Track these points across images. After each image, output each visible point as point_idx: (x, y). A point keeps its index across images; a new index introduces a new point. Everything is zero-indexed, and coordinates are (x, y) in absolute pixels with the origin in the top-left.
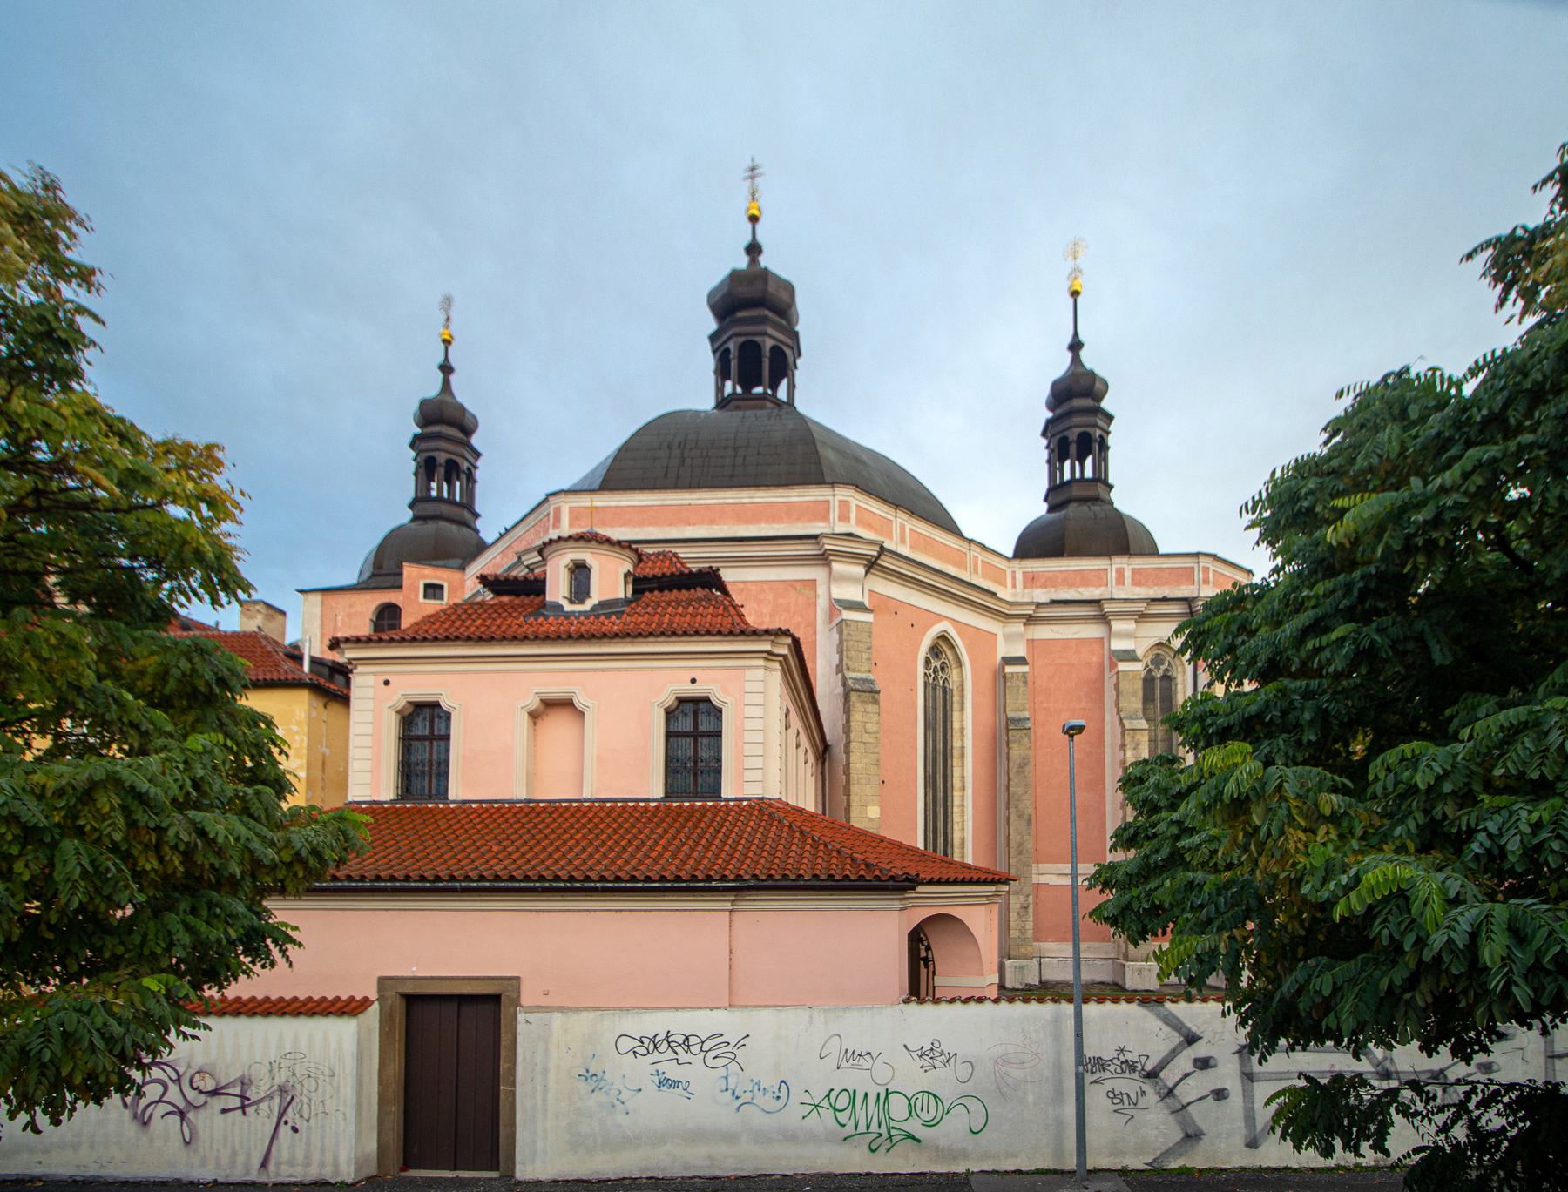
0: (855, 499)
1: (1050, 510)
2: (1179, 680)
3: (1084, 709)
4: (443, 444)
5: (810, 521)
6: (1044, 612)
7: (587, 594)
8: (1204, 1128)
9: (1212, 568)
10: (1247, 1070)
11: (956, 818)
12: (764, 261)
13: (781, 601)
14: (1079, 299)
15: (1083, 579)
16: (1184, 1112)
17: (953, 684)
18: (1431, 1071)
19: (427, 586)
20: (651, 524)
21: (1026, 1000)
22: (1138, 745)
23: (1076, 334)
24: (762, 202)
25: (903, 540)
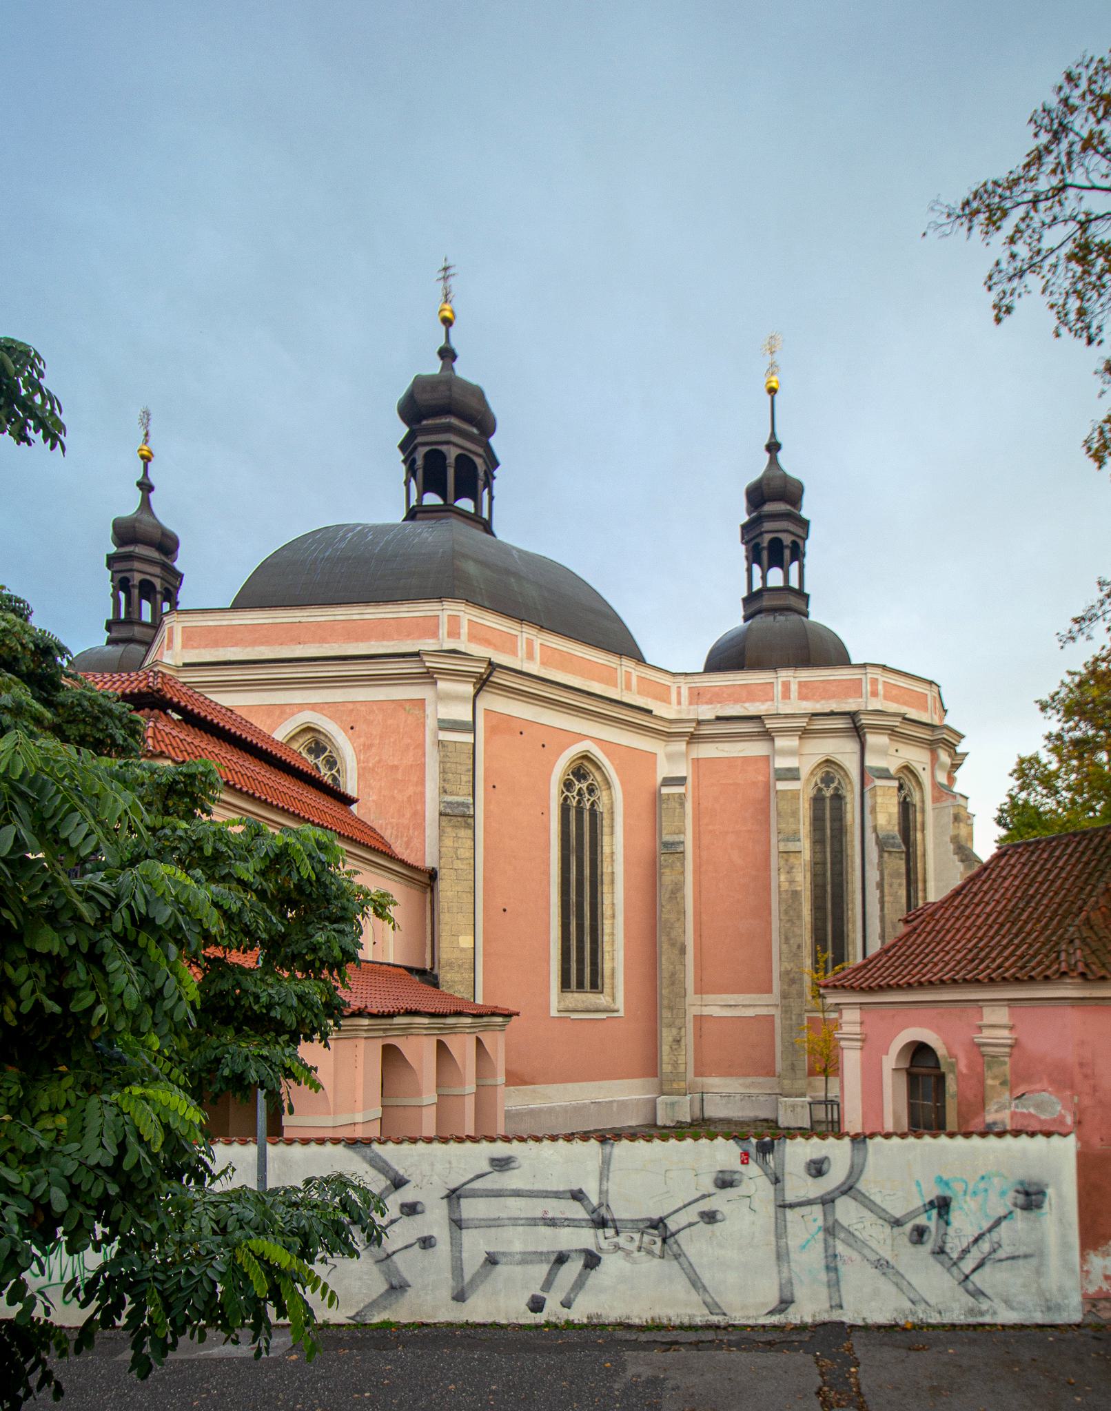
0: (466, 614)
1: (746, 619)
2: (848, 799)
3: (749, 831)
4: (137, 565)
5: (420, 637)
8: (408, 1277)
9: (881, 679)
10: (456, 1217)
11: (607, 948)
12: (462, 370)
13: (390, 722)
14: (777, 397)
15: (750, 694)
16: (389, 1261)
17: (601, 808)
18: (650, 1220)
20: (262, 644)
21: (680, 1138)
22: (792, 868)
23: (773, 434)
24: (457, 304)
25: (530, 656)
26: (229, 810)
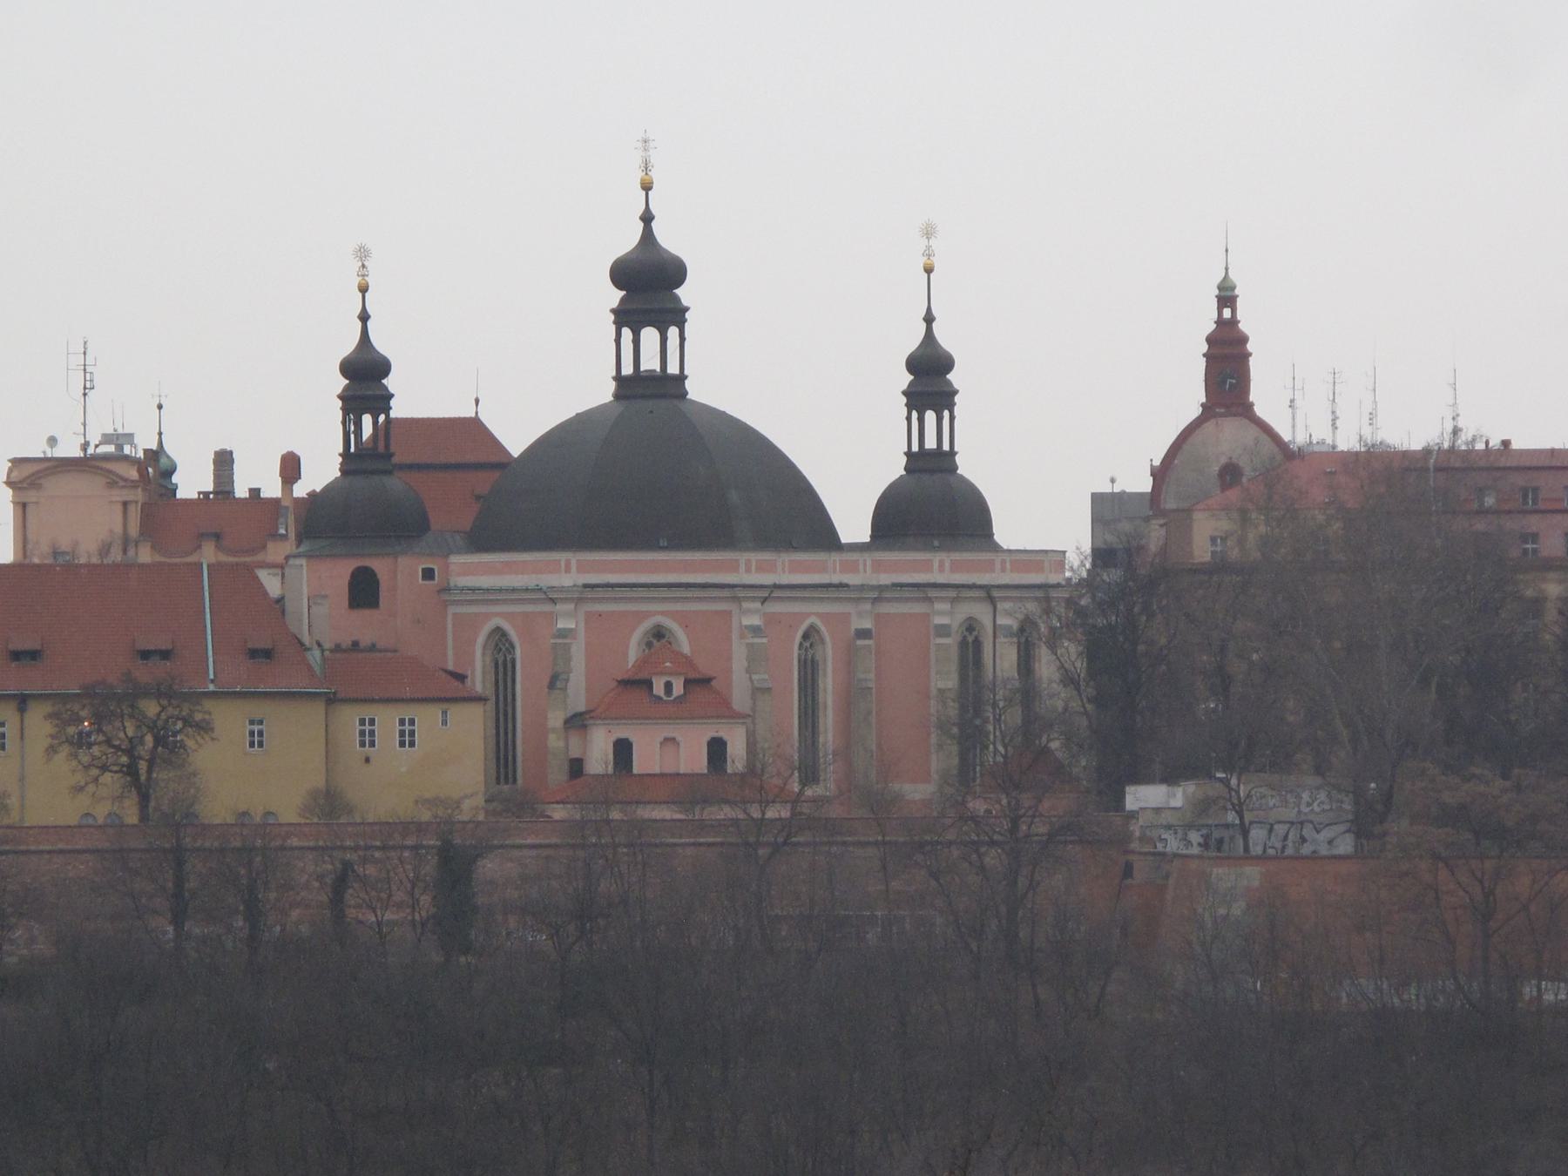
6: (887, 595)
7: (672, 695)
9: (1008, 559)
17: (818, 657)
19: (424, 570)
26: (803, 599)
